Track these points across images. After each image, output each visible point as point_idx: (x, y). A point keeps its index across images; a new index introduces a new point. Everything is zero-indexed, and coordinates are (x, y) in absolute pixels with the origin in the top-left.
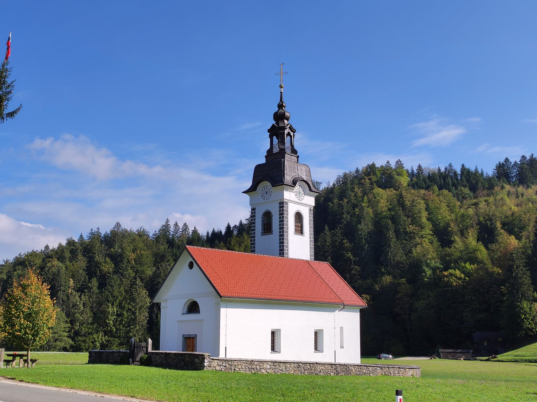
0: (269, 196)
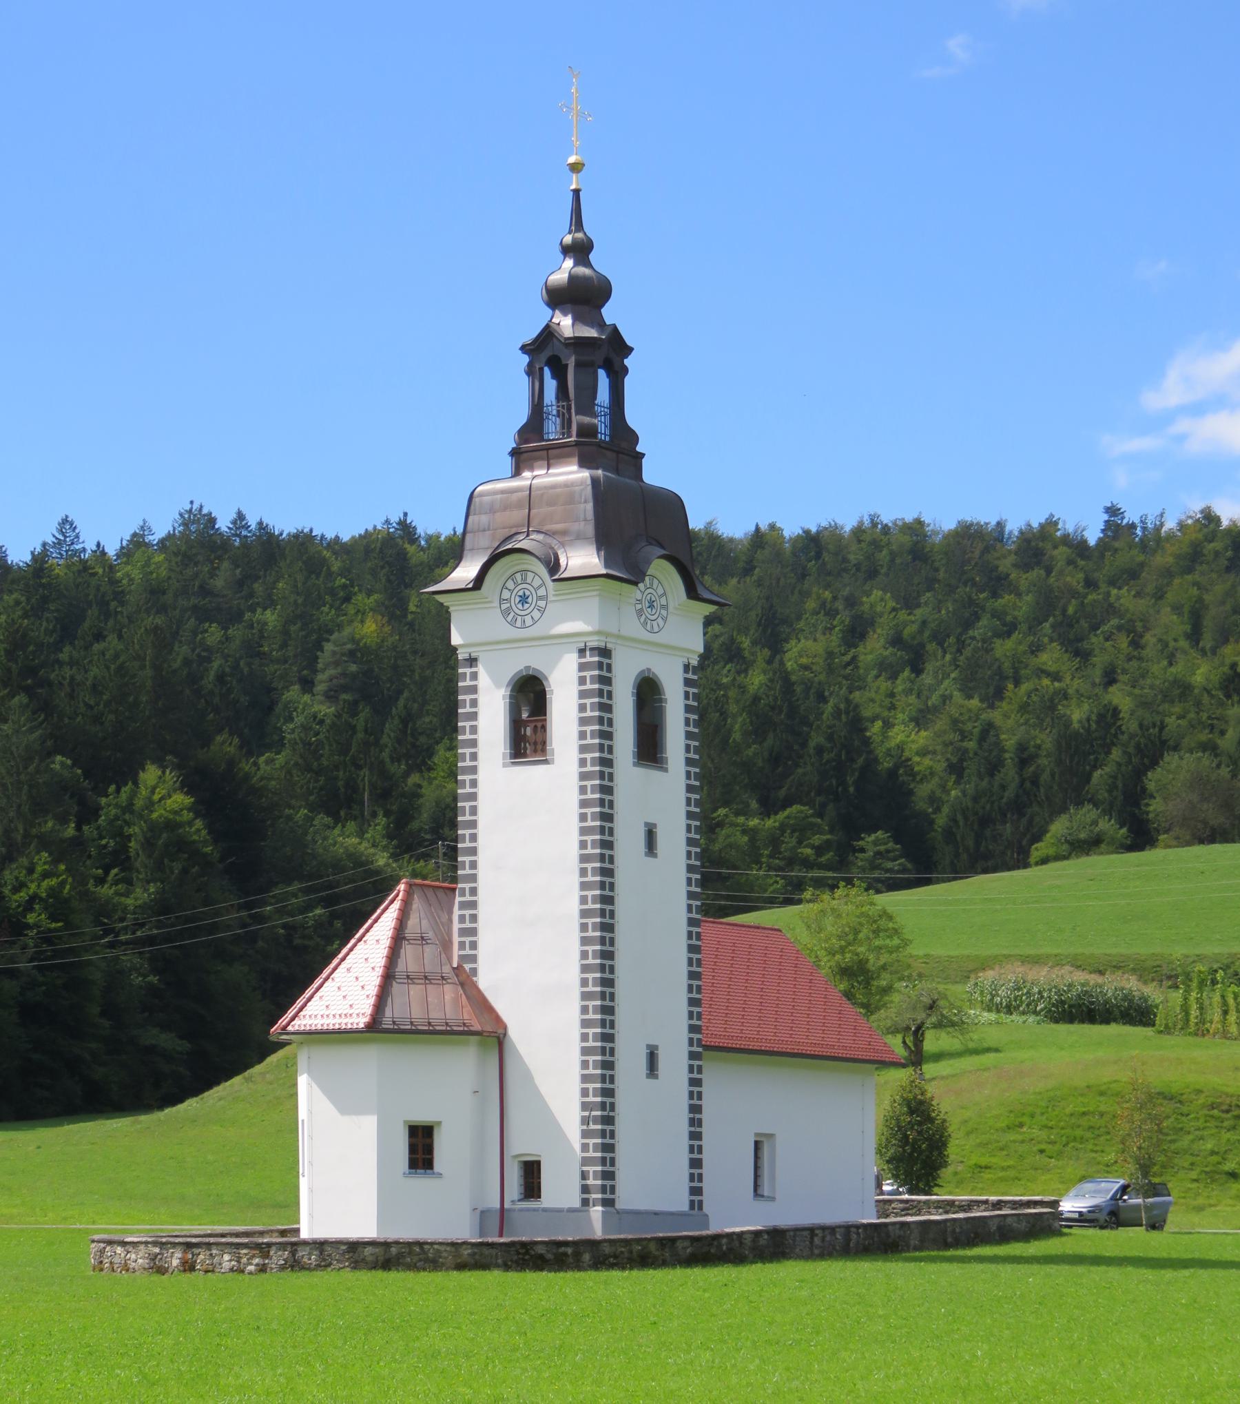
0: (536, 614)
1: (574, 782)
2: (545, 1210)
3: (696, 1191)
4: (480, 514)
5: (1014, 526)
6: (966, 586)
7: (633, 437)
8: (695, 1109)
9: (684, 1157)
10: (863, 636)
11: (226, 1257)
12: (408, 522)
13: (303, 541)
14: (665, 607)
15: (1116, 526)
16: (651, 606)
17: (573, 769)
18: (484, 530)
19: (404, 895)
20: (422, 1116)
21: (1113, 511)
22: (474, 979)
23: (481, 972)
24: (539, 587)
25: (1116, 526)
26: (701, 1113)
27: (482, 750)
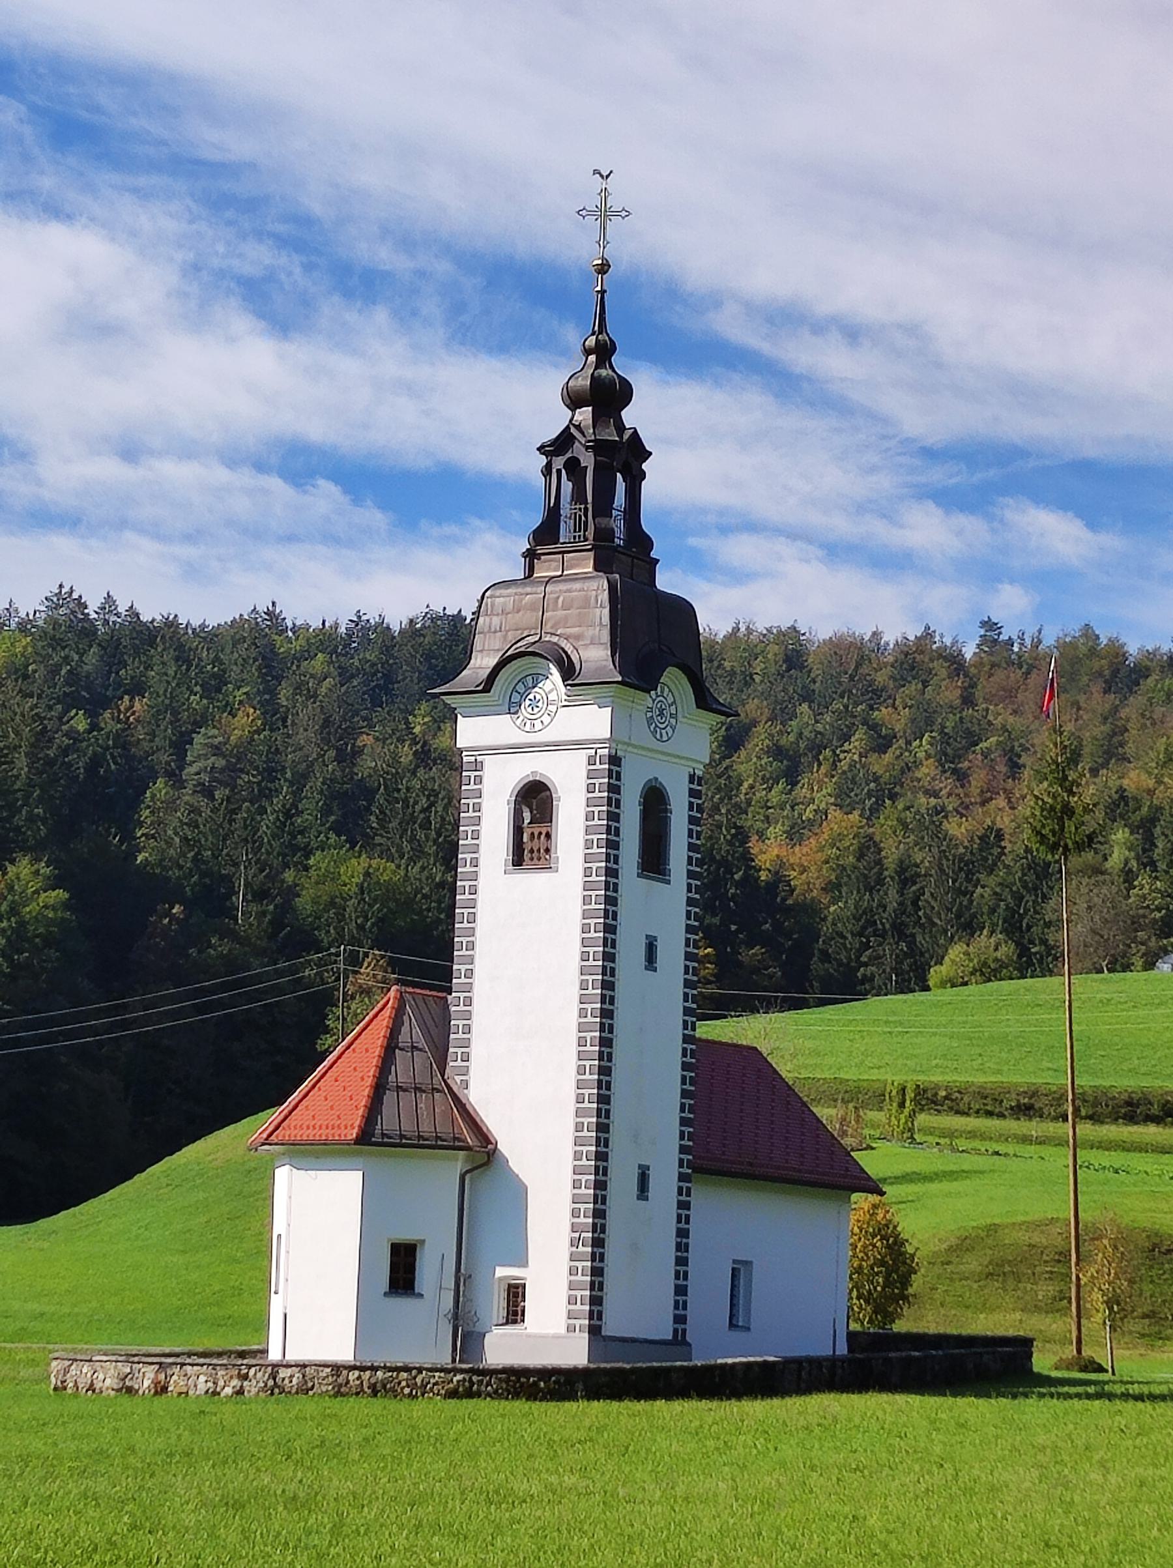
0: (546, 719)
1: (578, 892)
2: (529, 1336)
3: (680, 1319)
4: (492, 614)
5: (890, 637)
6: (843, 698)
7: (648, 543)
8: (682, 1233)
9: (670, 1283)
10: (737, 748)
11: (202, 1378)
12: (278, 611)
13: (171, 624)
16: (661, 714)
17: (578, 878)
18: (495, 632)
19: (394, 1003)
20: (405, 1235)
21: (990, 625)
22: (465, 1091)
24: (551, 691)
26: (688, 1237)
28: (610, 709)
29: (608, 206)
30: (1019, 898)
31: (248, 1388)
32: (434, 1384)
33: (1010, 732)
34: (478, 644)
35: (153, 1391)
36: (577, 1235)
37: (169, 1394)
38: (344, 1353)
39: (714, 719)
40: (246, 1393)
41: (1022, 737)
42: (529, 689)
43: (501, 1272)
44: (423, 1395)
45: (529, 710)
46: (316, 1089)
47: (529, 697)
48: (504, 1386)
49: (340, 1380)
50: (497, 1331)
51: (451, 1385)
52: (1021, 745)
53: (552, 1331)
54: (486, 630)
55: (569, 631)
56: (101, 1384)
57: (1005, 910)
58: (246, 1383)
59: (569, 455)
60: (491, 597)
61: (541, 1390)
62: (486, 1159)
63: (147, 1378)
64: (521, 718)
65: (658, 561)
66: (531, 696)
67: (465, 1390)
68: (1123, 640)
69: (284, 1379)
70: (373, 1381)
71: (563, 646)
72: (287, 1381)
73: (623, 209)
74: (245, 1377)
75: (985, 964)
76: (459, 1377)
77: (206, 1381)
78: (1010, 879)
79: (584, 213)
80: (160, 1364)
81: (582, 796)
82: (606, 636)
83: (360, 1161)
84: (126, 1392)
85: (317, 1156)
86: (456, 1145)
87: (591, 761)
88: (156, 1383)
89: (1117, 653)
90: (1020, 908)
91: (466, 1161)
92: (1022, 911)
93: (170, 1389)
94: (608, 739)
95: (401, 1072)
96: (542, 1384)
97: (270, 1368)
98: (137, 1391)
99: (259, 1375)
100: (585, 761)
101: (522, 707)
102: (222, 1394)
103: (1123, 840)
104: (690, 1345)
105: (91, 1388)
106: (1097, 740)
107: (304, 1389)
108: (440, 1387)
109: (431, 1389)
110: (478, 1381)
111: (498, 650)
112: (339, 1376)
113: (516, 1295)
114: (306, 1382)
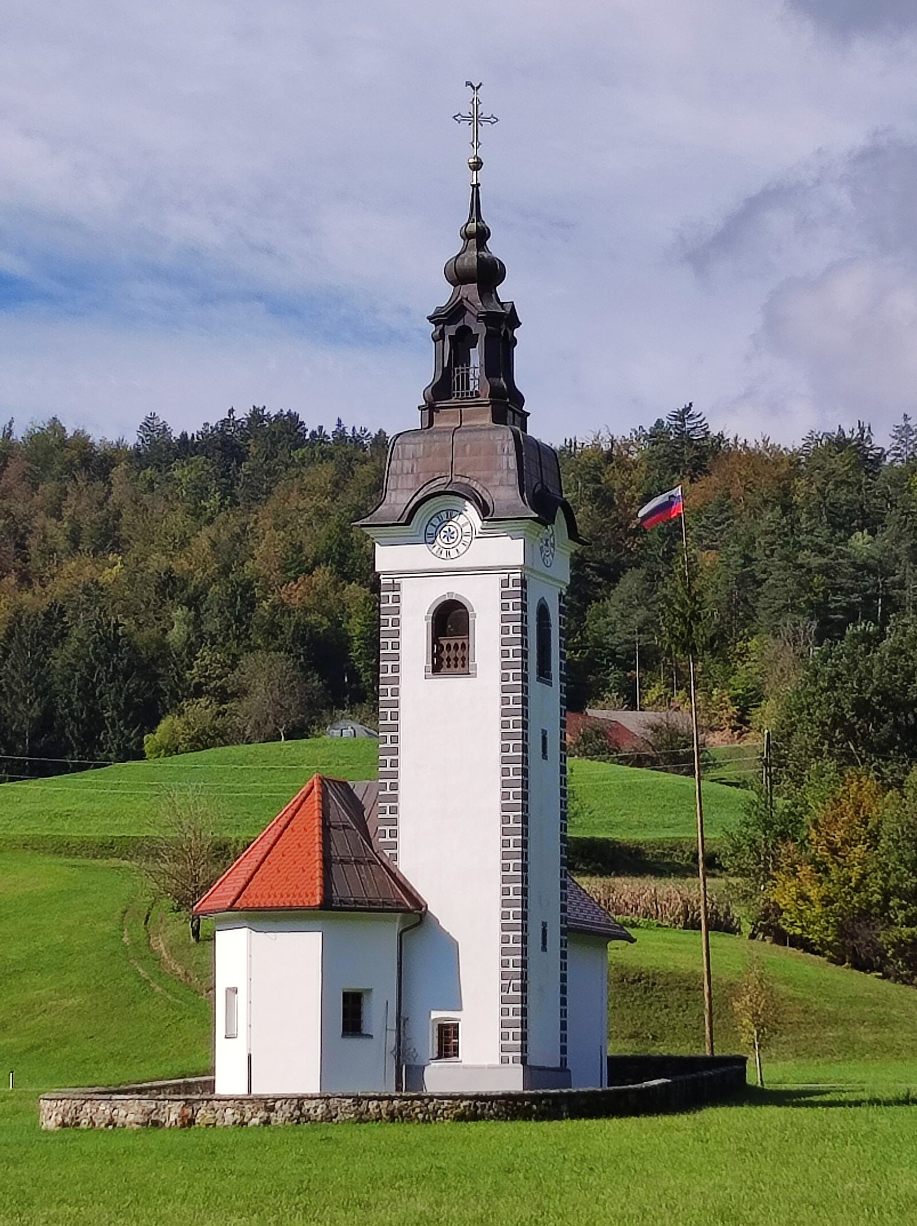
0: (461, 548)
2: (464, 1067)
4: (403, 458)
11: (229, 1111)
14: (553, 545)
15: (340, 434)
18: (408, 473)
20: (355, 985)
22: (395, 863)
23: (401, 857)
25: (340, 434)
27: (404, 663)
28: (522, 540)
29: (479, 113)
30: (92, 669)
31: (274, 1118)
32: (444, 1110)
33: (14, 517)
34: (391, 484)
35: (179, 1125)
36: (508, 982)
37: (197, 1125)
38: (314, 1088)
39: (575, 546)
40: (272, 1123)
41: (25, 521)
42: (443, 523)
43: (435, 1015)
44: (434, 1119)
45: (445, 540)
46: (266, 863)
47: (445, 529)
48: (504, 1109)
49: (361, 1109)
50: (434, 1064)
51: (459, 1110)
52: (25, 528)
53: (486, 1063)
54: (398, 472)
55: (478, 474)
56: (123, 1119)
57: (80, 679)
58: (272, 1114)
59: (460, 324)
60: (401, 444)
61: (534, 1112)
62: (418, 920)
63: (173, 1112)
64: (437, 547)
65: (528, 414)
66: (446, 529)
67: (471, 1114)
68: (88, 432)
69: (308, 1110)
70: (390, 1109)
71: (474, 486)
72: (312, 1111)
73: (492, 116)
74: (272, 1109)
75: (204, 732)
76: (465, 1103)
77: (233, 1114)
78: (83, 651)
79: (458, 118)
80: (186, 1100)
81: (497, 613)
82: (513, 479)
83: (319, 924)
84: (152, 1125)
85: (276, 920)
86: (398, 909)
87: (504, 584)
88: (183, 1117)
89: (82, 443)
90: (93, 677)
91: (403, 920)
92: (94, 680)
93: (197, 1121)
94: (521, 567)
95: (339, 849)
96: (534, 1107)
97: (295, 1101)
98: (163, 1124)
99: (284, 1107)
100: (499, 584)
101: (438, 538)
102: (250, 1124)
103: (182, 617)
104: (569, 1071)
105: (112, 1122)
106: (96, 524)
107: (329, 1117)
108: (449, 1112)
109: (442, 1114)
110: (482, 1106)
111: (411, 489)
112: (360, 1106)
113: (447, 1034)
114: (330, 1111)
